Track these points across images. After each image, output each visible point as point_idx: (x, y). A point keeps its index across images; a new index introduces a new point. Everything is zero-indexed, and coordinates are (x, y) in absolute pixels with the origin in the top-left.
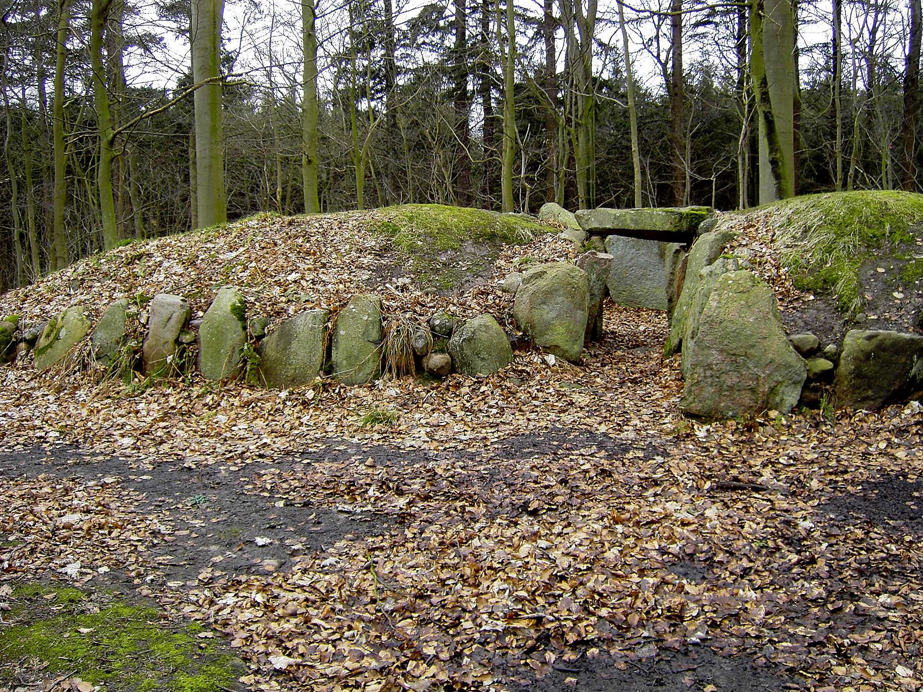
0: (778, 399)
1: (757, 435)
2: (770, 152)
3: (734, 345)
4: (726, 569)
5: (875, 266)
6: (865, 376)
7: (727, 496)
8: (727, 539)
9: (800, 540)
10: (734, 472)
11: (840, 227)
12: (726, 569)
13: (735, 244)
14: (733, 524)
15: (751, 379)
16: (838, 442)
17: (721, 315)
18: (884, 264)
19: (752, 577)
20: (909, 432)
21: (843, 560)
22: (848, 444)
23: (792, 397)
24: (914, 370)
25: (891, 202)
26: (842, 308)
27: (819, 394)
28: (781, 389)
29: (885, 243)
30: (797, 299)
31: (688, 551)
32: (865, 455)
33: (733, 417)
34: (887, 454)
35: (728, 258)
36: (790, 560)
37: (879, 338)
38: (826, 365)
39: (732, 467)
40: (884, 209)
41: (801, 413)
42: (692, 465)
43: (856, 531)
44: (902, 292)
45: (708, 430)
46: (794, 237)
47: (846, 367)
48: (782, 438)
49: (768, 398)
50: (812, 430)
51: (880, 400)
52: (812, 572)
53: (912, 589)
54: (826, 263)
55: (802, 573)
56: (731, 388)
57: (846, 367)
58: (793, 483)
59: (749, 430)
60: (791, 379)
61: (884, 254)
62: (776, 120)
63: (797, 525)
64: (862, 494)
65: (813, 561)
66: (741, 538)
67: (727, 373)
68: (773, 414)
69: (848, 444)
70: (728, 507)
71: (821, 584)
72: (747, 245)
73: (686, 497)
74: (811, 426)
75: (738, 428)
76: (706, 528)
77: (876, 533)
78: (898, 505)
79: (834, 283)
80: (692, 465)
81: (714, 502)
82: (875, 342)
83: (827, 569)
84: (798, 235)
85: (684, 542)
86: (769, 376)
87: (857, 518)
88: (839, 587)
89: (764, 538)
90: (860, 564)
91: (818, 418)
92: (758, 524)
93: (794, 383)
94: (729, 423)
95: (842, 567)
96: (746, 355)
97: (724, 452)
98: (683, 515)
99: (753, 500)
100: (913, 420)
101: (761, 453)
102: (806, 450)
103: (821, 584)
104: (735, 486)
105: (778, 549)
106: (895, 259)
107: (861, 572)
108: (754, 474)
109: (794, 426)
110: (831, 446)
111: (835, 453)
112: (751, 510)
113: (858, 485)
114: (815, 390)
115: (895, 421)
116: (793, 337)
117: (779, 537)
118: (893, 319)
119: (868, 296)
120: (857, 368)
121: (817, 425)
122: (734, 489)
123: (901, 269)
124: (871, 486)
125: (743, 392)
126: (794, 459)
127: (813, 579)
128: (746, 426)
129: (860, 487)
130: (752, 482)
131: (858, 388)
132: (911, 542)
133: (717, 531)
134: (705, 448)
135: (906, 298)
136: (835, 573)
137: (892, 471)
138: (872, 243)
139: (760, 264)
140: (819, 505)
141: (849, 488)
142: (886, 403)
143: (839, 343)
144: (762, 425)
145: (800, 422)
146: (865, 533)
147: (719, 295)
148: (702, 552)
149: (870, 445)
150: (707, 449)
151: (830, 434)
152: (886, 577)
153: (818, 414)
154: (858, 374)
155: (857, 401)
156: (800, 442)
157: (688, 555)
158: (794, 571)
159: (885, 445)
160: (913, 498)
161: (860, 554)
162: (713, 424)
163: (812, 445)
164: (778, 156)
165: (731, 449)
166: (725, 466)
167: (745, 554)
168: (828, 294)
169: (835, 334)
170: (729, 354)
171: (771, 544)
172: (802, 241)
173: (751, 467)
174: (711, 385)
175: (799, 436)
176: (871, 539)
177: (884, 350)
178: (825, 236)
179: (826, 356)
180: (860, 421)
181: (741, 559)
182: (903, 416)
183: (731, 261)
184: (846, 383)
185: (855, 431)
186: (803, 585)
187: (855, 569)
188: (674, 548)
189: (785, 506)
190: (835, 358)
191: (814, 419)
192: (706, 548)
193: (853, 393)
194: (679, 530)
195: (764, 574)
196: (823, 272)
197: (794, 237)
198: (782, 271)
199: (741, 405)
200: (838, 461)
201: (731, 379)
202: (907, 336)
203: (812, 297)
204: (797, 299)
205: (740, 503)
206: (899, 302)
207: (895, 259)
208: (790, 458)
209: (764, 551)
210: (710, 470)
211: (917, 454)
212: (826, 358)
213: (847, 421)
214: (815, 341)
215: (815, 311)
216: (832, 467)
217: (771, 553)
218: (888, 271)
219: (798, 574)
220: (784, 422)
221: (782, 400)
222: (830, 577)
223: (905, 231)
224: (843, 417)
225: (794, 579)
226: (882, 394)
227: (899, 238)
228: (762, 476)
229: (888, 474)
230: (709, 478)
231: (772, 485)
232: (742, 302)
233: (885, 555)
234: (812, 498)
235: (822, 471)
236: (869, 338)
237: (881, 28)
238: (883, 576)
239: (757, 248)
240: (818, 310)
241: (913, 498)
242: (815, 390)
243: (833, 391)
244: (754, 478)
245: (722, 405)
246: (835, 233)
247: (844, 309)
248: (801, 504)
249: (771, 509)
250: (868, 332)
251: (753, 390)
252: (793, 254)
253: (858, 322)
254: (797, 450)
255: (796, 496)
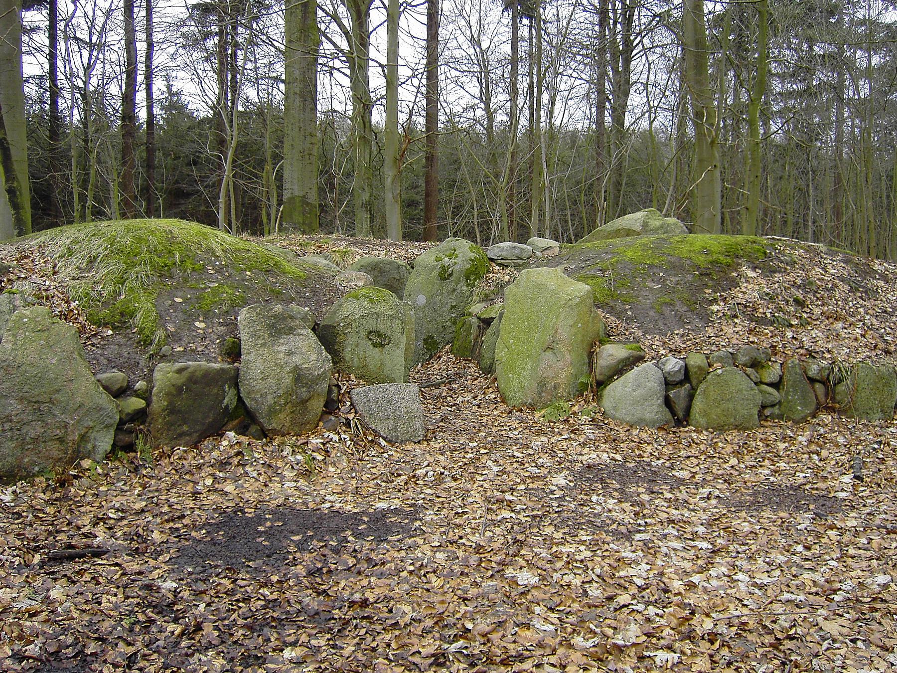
0: (89, 446)
1: (73, 490)
2: (7, 181)
3: (37, 391)
4: (105, 661)
5: (171, 296)
6: (179, 411)
7: (69, 568)
8: (91, 623)
9: (168, 605)
10: (62, 537)
11: (130, 257)
12: (105, 661)
13: (12, 277)
14: (87, 602)
15: (58, 428)
16: (163, 485)
17: (19, 359)
18: (180, 294)
19: (141, 665)
20: (230, 464)
21: (225, 619)
22: (174, 485)
23: (104, 442)
24: (226, 399)
25: (176, 231)
26: (145, 341)
27: (134, 435)
28: (93, 435)
29: (177, 272)
30: (95, 335)
31: (51, 649)
32: (195, 495)
33: (41, 473)
34: (216, 490)
35: (14, 293)
36: (173, 633)
37: (189, 370)
38: (139, 403)
39: (58, 532)
40: (171, 238)
41: (117, 459)
42: (11, 538)
43: (222, 581)
44: (203, 321)
45: (14, 492)
46: (79, 268)
47: (158, 404)
48: (102, 489)
49: (79, 446)
50: (132, 475)
51: (195, 435)
52: (204, 642)
53: (309, 636)
54: (120, 295)
55: (193, 645)
56: (35, 440)
57: (158, 404)
58: (132, 539)
59: (62, 485)
60: (103, 423)
61: (178, 282)
62: (11, 147)
63: (159, 588)
64: (209, 539)
65: (199, 628)
66: (105, 618)
67: (29, 423)
68: (86, 463)
69: (174, 485)
70: (74, 582)
71: (218, 654)
72: (26, 278)
73: (18, 580)
74: (130, 471)
75: (49, 485)
76: (59, 615)
77: (243, 579)
78: (249, 544)
79: (132, 315)
80: (11, 538)
81: (55, 580)
82: (186, 374)
83: (216, 633)
84: (83, 266)
85: (41, 639)
86: (78, 421)
87: (216, 566)
88: (239, 652)
89: (131, 612)
90: (246, 619)
91: (136, 462)
92: (115, 595)
93: (106, 427)
94: (37, 480)
95: (229, 627)
96: (51, 401)
97: (41, 515)
98: (24, 604)
99: (98, 568)
100: (233, 452)
101: (83, 509)
102: (132, 499)
103: (218, 654)
104: (70, 554)
105: (152, 621)
106: (191, 288)
107: (250, 628)
108: (86, 536)
109: (112, 474)
110: (157, 491)
111: (164, 497)
112: (101, 580)
113: (201, 529)
114: (130, 432)
115: (215, 454)
116: (100, 376)
117: (148, 607)
118: (199, 349)
119: (171, 328)
120: (171, 403)
121: (136, 470)
122: (71, 558)
123: (198, 298)
124: (213, 527)
125: (50, 444)
126: (123, 511)
127: (207, 649)
128: (58, 481)
129: (204, 531)
130: (89, 546)
131: (172, 425)
132: (279, 582)
133: (75, 615)
134: (16, 513)
135: (207, 327)
136: (226, 636)
137: (228, 507)
138: (164, 272)
139: (47, 298)
140: (170, 559)
141: (194, 534)
142: (204, 436)
143: (149, 378)
144: (76, 477)
145: (117, 468)
146: (233, 582)
147: (14, 336)
148: (67, 647)
149: (196, 483)
150: (19, 515)
151: (151, 477)
152: (275, 627)
153: (136, 457)
154: (172, 410)
155: (172, 439)
156: (122, 491)
157: (53, 653)
158: (183, 644)
159: (211, 481)
160: (260, 534)
161: (240, 607)
162: (19, 484)
163: (136, 492)
164: (15, 185)
165: (48, 510)
166: (50, 533)
167: (119, 637)
168: (127, 328)
169: (142, 370)
170: (30, 402)
171: (141, 617)
172: (88, 272)
173: (79, 528)
174: (11, 439)
175: (120, 484)
176: (241, 587)
177: (195, 383)
178: (115, 266)
179: (137, 394)
180: (180, 459)
181: (116, 644)
182: (222, 448)
183: (18, 296)
184: (160, 420)
185: (176, 470)
186: (200, 660)
187: (244, 626)
188: (33, 650)
189: (136, 567)
190: (146, 395)
191: (132, 463)
192: (70, 640)
193: (169, 430)
194: (28, 623)
195: (153, 657)
196: (118, 305)
197: (79, 268)
198: (73, 305)
199: (48, 458)
200: (170, 506)
201: (33, 431)
202: (217, 366)
203: (110, 332)
204: (95, 335)
205: (86, 575)
206: (202, 332)
207: (191, 288)
208: (118, 510)
209: (137, 628)
210: (34, 540)
211: (245, 486)
212: (138, 396)
213: (167, 461)
214: (124, 379)
215: (116, 347)
216: (166, 514)
217: (146, 629)
218: (186, 300)
219: (189, 648)
220: (100, 471)
221: (94, 447)
222: (223, 642)
223: (195, 259)
224: (161, 457)
225: (187, 655)
226: (197, 427)
227: (190, 267)
228: (96, 537)
229: (225, 512)
230: (36, 549)
231: (111, 546)
232: (42, 342)
233: (263, 603)
234: (160, 553)
235: (158, 520)
236: (180, 371)
237: (99, 66)
238: (272, 627)
239: (39, 281)
240: (120, 345)
241: (260, 534)
242: (130, 432)
243: (148, 430)
244: (89, 541)
245: (26, 460)
246: (125, 263)
247: (147, 342)
248: (152, 562)
249: (123, 574)
250: (178, 365)
251: (61, 440)
252: (82, 286)
253: (164, 356)
254: (123, 500)
255: (143, 554)
